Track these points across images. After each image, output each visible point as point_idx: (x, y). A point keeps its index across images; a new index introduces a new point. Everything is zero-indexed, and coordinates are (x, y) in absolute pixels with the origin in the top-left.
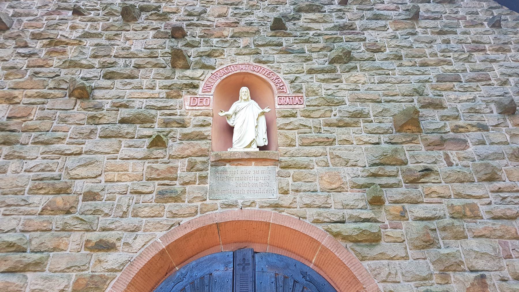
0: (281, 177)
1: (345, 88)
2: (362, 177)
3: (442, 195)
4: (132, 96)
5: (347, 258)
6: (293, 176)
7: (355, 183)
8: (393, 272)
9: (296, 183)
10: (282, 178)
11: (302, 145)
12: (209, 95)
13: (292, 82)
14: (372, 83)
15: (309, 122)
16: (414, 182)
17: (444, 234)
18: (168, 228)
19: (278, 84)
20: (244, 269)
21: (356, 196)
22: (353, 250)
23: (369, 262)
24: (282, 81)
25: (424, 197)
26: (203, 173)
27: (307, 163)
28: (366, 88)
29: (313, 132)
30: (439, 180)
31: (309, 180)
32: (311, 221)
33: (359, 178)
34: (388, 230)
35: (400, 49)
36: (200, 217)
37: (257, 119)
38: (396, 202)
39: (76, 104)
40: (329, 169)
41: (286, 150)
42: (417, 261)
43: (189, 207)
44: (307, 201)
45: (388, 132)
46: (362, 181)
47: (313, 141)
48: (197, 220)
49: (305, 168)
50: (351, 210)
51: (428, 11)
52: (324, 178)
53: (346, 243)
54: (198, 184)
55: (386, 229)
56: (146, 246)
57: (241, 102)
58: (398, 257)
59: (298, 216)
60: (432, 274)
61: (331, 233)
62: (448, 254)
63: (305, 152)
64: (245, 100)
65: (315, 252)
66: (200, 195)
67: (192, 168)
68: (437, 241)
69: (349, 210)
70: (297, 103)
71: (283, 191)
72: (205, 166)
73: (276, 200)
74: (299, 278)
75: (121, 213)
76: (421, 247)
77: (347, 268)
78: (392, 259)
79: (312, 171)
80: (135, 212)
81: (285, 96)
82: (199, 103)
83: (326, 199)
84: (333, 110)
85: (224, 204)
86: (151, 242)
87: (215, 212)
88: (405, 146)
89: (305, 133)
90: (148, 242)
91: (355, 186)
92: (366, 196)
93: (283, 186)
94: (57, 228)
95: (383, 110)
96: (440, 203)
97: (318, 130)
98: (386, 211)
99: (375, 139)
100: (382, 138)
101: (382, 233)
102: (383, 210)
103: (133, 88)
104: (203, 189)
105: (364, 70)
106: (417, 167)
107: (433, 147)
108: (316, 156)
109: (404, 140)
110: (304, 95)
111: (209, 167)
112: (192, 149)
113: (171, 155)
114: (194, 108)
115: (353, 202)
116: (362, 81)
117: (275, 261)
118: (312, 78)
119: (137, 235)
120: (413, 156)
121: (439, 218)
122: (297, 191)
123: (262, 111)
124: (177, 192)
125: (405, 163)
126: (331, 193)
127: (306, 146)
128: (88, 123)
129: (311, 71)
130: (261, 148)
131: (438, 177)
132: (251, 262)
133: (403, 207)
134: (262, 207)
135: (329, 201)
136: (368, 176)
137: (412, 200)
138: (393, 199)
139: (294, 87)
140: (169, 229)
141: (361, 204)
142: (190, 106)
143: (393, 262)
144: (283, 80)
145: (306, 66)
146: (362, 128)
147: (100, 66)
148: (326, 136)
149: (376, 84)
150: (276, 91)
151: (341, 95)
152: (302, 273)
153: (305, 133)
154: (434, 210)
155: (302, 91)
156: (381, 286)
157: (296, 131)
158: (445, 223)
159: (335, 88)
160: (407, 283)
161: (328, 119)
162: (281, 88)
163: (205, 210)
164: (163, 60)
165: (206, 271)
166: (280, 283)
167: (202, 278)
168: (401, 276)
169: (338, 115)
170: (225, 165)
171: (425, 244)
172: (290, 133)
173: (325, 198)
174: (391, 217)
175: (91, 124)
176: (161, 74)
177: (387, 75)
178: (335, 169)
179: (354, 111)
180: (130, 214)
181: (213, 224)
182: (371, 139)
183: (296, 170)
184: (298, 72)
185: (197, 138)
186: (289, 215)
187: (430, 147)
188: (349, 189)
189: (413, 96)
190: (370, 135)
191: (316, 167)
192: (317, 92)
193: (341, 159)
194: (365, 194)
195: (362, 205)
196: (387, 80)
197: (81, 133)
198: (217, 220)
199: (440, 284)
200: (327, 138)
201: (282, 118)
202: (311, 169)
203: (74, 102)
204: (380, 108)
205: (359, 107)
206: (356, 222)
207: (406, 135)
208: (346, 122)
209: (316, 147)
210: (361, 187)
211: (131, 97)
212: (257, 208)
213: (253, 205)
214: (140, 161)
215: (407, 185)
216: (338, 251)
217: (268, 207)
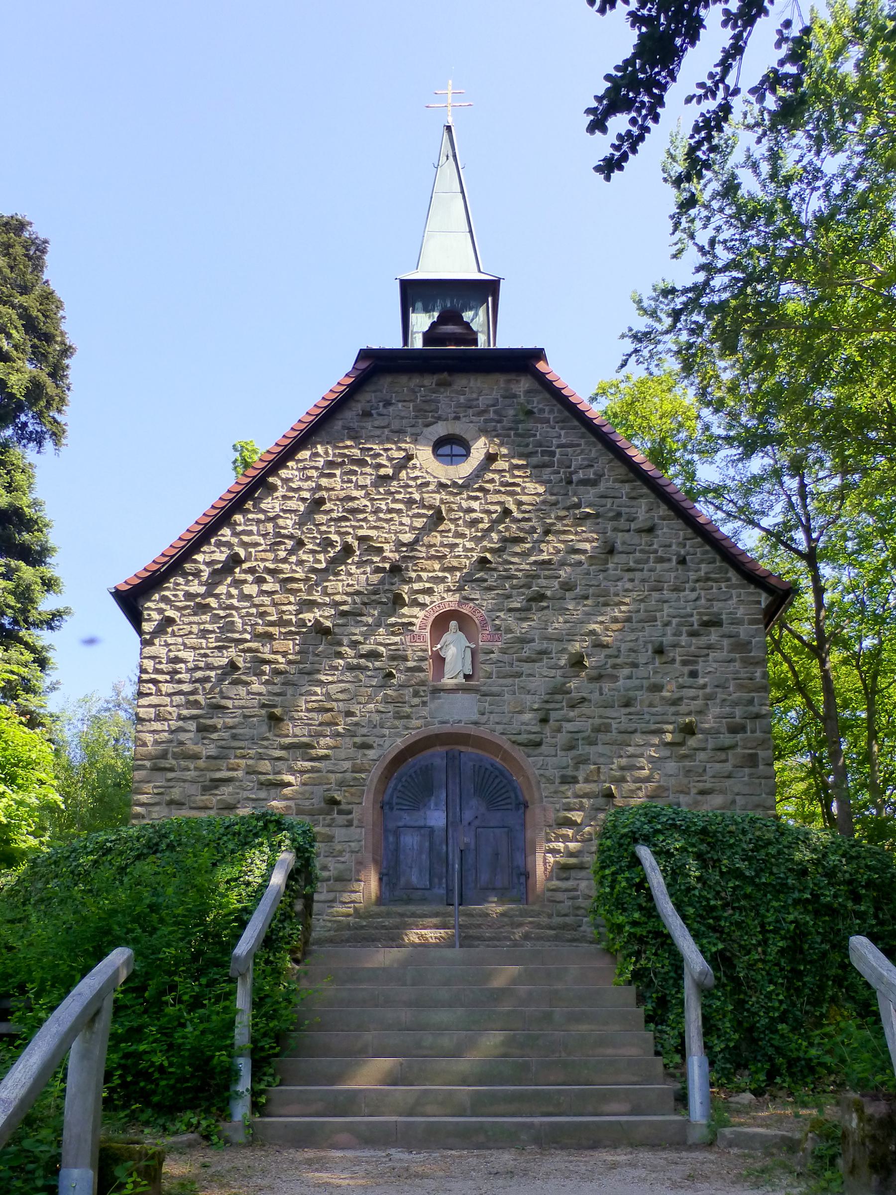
16: (573, 707)
26: (425, 699)
51: (624, 543)
97: (511, 665)
130: (467, 677)
141: (534, 722)
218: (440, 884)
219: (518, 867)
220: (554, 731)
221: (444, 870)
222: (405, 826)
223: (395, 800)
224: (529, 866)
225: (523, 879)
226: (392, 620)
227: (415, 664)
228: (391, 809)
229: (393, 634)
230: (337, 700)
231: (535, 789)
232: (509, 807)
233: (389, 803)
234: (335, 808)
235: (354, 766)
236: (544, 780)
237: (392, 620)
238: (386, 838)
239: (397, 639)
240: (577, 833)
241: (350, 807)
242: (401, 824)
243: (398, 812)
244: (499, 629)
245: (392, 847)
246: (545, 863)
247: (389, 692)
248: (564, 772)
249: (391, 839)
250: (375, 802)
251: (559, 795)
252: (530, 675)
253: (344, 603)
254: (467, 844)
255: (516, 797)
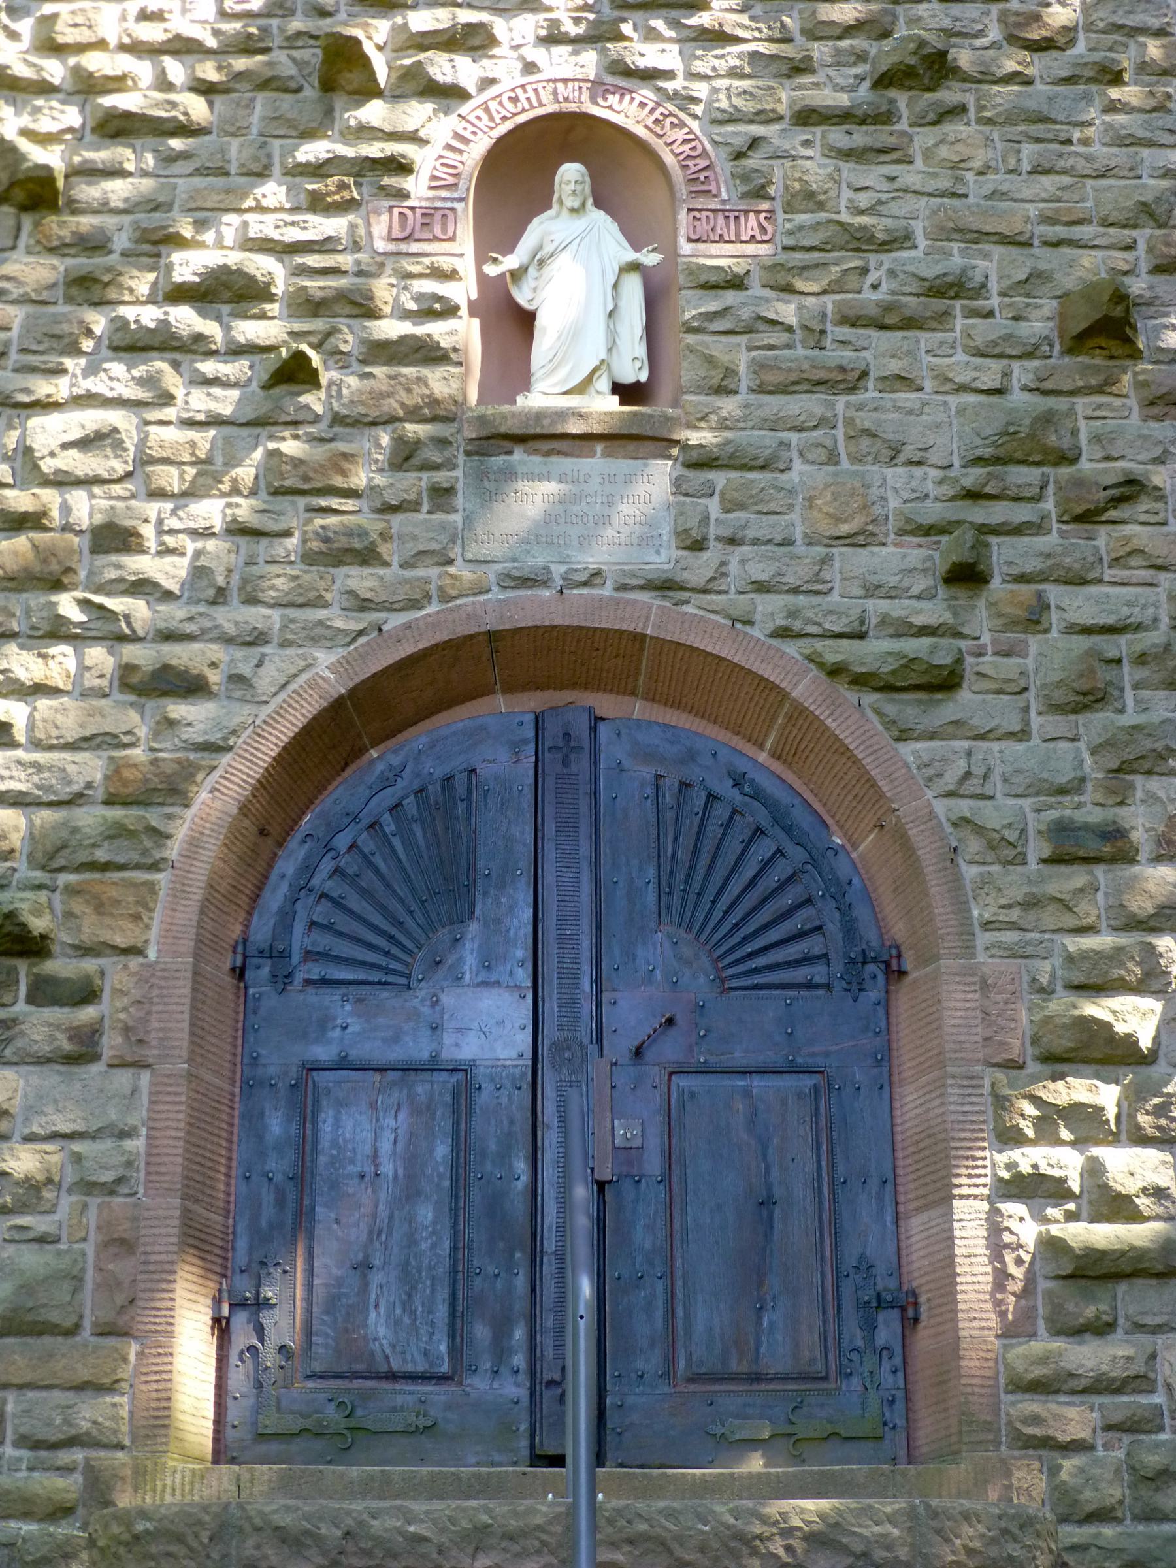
0: (687, 495)
1: (918, 187)
2: (936, 499)
3: (1159, 562)
4: (199, 204)
5: (858, 733)
6: (722, 494)
7: (908, 520)
8: (978, 770)
9: (731, 516)
10: (688, 500)
11: (761, 389)
12: (452, 200)
13: (739, 155)
14: (1011, 172)
15: (787, 311)
16: (1087, 517)
17: (1142, 673)
18: (348, 639)
19: (690, 163)
20: (565, 762)
21: (908, 559)
22: (877, 711)
23: (919, 745)
24: (704, 149)
25: (1106, 565)
27: (768, 452)
28: (987, 189)
29: (799, 346)
30: (1162, 515)
31: (772, 506)
32: (768, 632)
33: (928, 504)
34: (986, 658)
35: (1124, 39)
36: (438, 612)
37: (615, 286)
38: (1022, 578)
39: (18, 229)
40: (836, 474)
41: (706, 406)
42: (1051, 745)
43: (407, 581)
44: (760, 572)
45: (1038, 353)
46: (932, 512)
47: (793, 377)
48: (430, 620)
49: (763, 467)
50: (888, 601)
52: (819, 502)
53: (861, 695)
54: (429, 512)
55: (980, 655)
56: (293, 686)
57: (558, 215)
58: (1000, 732)
59: (728, 616)
60: (1083, 780)
61: (821, 665)
62: (1134, 727)
63: (766, 412)
64: (573, 210)
65: (773, 719)
66: (434, 546)
67: (407, 459)
68: (1116, 693)
69: (882, 601)
70: (753, 237)
71: (688, 542)
72: (447, 454)
73: (666, 567)
74: (724, 788)
75: (211, 592)
76: (1068, 708)
77: (856, 761)
78: (982, 737)
79: (784, 477)
80: (249, 589)
81: (713, 207)
82: (418, 227)
83: (817, 568)
84: (872, 265)
85: (508, 575)
86: (304, 677)
87: (482, 598)
88: (1082, 404)
89: (771, 348)
90: (295, 676)
91: (909, 527)
92: (937, 561)
93: (688, 526)
94: (33, 628)
95: (1031, 275)
96: (1151, 585)
98: (991, 605)
99: (989, 374)
100: (1015, 374)
101: (968, 668)
102: (981, 603)
103: (198, 172)
104: (443, 527)
105: (990, 121)
106: (1105, 471)
107: (1166, 409)
108: (800, 429)
109: (1080, 383)
110: (778, 205)
111: (461, 459)
112: (403, 395)
113: (337, 414)
114: (404, 247)
115: (897, 578)
116: (977, 164)
117: (657, 742)
118: (807, 143)
119: (263, 655)
120: (1096, 439)
121: (1138, 627)
122: (732, 541)
123: (631, 256)
124: (366, 534)
125: (1068, 458)
126: (835, 550)
127: (771, 393)
128: (69, 300)
129: (806, 117)
130: (627, 392)
131: (1159, 505)
132: (586, 743)
133: (1040, 595)
134: (623, 588)
135: (825, 575)
136: (953, 498)
137: (1071, 574)
138: (1015, 571)
139: (745, 178)
140: (350, 643)
141: (920, 584)
142: (392, 239)
143: (984, 745)
144: (708, 147)
145: (785, 98)
146: (958, 334)
147: (80, 87)
148: (838, 362)
149: (1024, 176)
150: (682, 190)
151: (902, 213)
152: (731, 774)
153: (771, 348)
154: (1129, 604)
155: (772, 191)
156: (941, 807)
157: (743, 339)
158: (1149, 643)
159: (885, 186)
160: (1012, 802)
161: (850, 300)
162: (702, 177)
163: (454, 593)
164: (290, 63)
165: (457, 763)
166: (668, 799)
167: (448, 779)
168: (999, 784)
169: (884, 287)
170: (510, 453)
171: (1079, 698)
172: (717, 347)
173: (814, 564)
174: (999, 622)
175: (80, 300)
176: (288, 120)
177: (1062, 143)
178: (856, 472)
179: (937, 277)
180: (235, 598)
181: (479, 634)
182: (977, 374)
183: (734, 474)
184: (763, 117)
185: (418, 356)
186: (701, 613)
187: (1155, 410)
188: (892, 536)
189: (1135, 227)
190: (979, 360)
191: (798, 465)
192: (822, 197)
193: (879, 444)
194: (937, 555)
195: (922, 587)
196: (1061, 164)
197: (53, 336)
198: (491, 622)
199: (1103, 805)
200: (842, 369)
201: (699, 292)
202: (782, 471)
203: (11, 222)
204: (1021, 265)
205: (956, 258)
206: (897, 635)
207: (1088, 367)
208: (908, 313)
209: (804, 396)
210: (928, 531)
211: (193, 205)
212: (607, 591)
213: (598, 581)
214: (245, 432)
215: (1064, 527)
216: (836, 714)
217: (642, 588)
218: (500, 1351)
219: (865, 1267)
220: (1012, 624)
221: (521, 1282)
222: (343, 1064)
223: (299, 938)
224: (918, 1264)
225: (887, 1329)
226: (312, 151)
227: (405, 328)
228: (283, 979)
229: (318, 204)
230: (63, 481)
231: (936, 888)
232: (818, 973)
233: (276, 954)
234: (22, 967)
235: (116, 771)
236: (974, 845)
237: (312, 151)
238: (253, 1120)
239: (334, 226)
240: (1134, 1097)
241: (89, 965)
242: (323, 1053)
243: (313, 997)
244: (760, 193)
245: (278, 1165)
246: (997, 1247)
247: (291, 447)
248: (1065, 809)
249: (276, 1125)
250: (203, 944)
251: (1050, 917)
252: (903, 381)
253: (118, 83)
254: (628, 1154)
255: (850, 930)
